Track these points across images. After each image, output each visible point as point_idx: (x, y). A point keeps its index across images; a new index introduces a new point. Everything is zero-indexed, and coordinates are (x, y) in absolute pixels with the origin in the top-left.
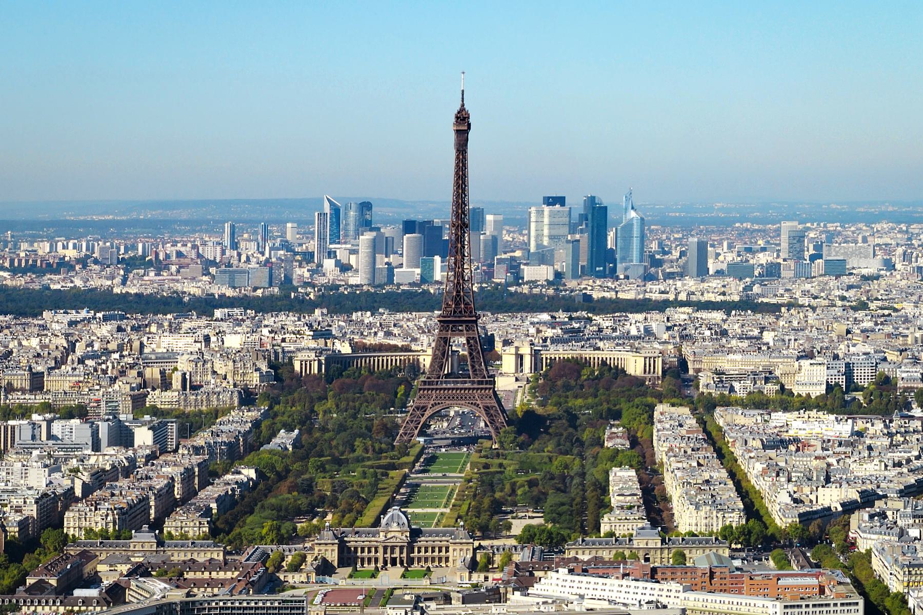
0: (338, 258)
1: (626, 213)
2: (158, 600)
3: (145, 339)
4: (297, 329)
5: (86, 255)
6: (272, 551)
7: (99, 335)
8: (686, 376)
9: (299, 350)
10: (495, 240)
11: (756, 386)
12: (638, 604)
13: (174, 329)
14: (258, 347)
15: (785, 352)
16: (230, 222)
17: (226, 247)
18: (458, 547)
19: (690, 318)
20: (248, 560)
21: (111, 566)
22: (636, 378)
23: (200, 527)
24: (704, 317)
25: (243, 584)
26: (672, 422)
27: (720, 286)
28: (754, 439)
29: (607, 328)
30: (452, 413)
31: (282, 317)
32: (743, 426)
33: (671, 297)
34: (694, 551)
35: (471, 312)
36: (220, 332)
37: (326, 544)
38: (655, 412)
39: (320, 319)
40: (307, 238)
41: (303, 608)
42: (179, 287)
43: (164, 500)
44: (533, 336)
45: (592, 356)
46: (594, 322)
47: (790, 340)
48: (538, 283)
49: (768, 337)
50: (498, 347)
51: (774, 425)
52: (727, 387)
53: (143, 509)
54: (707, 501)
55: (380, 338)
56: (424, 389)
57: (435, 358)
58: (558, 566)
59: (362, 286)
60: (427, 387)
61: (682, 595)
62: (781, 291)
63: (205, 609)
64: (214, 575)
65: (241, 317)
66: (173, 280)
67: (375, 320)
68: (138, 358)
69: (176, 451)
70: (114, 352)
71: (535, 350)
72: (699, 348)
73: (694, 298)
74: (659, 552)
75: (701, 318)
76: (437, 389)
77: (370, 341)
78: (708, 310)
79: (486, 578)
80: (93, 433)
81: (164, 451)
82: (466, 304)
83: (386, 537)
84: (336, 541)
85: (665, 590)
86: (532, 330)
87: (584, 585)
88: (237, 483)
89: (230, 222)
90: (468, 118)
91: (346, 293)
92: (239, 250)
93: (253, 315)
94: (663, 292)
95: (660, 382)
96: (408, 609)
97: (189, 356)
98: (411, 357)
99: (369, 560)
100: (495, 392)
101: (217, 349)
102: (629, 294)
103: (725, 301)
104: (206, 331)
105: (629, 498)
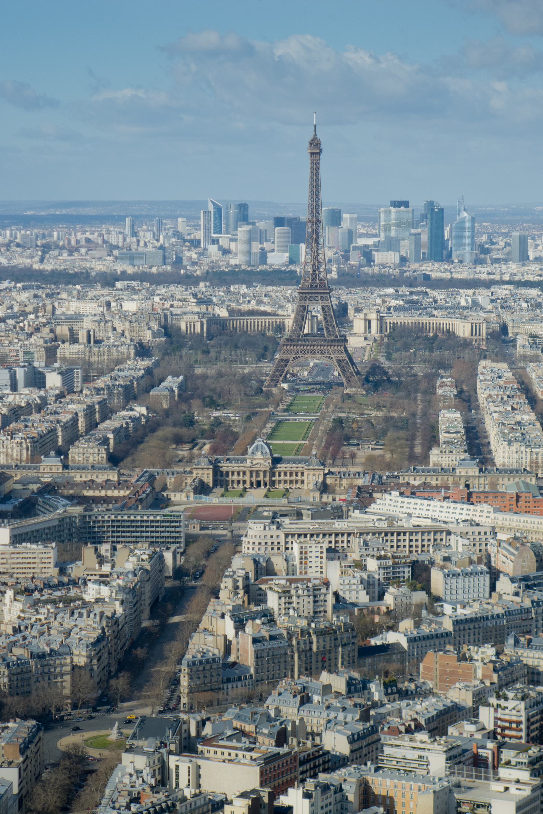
0: (220, 244)
2: (60, 514)
3: (56, 304)
5: (10, 240)
6: (158, 473)
7: (18, 300)
8: (506, 338)
9: (185, 313)
10: (350, 232)
12: (456, 522)
13: (81, 297)
14: (150, 311)
18: (311, 473)
19: (511, 293)
20: (137, 481)
21: (24, 485)
22: (465, 340)
23: (98, 454)
24: (523, 292)
25: (133, 501)
26: (493, 375)
30: (312, 364)
31: (172, 288)
33: (497, 277)
34: (506, 479)
36: (119, 299)
37: (203, 469)
39: (204, 290)
40: (196, 229)
41: (180, 521)
42: (88, 265)
44: (379, 305)
50: (351, 312)
53: (51, 438)
55: (253, 305)
57: (296, 320)
58: (392, 489)
59: (241, 265)
60: (289, 343)
61: (492, 515)
63: (99, 521)
64: (110, 493)
66: (82, 259)
67: (250, 292)
68: (50, 319)
70: (30, 313)
73: (516, 278)
74: (477, 479)
77: (246, 307)
79: (334, 500)
80: (11, 376)
81: (71, 391)
82: (321, 280)
83: (252, 463)
84: (211, 467)
85: (479, 511)
86: (379, 301)
87: (412, 506)
88: (130, 418)
90: (320, 144)
91: (227, 270)
92: (138, 238)
94: (489, 273)
95: (484, 343)
96: (267, 524)
98: (278, 321)
100: (346, 350)
101: (116, 312)
102: (462, 274)
104: (108, 298)
105: (454, 435)
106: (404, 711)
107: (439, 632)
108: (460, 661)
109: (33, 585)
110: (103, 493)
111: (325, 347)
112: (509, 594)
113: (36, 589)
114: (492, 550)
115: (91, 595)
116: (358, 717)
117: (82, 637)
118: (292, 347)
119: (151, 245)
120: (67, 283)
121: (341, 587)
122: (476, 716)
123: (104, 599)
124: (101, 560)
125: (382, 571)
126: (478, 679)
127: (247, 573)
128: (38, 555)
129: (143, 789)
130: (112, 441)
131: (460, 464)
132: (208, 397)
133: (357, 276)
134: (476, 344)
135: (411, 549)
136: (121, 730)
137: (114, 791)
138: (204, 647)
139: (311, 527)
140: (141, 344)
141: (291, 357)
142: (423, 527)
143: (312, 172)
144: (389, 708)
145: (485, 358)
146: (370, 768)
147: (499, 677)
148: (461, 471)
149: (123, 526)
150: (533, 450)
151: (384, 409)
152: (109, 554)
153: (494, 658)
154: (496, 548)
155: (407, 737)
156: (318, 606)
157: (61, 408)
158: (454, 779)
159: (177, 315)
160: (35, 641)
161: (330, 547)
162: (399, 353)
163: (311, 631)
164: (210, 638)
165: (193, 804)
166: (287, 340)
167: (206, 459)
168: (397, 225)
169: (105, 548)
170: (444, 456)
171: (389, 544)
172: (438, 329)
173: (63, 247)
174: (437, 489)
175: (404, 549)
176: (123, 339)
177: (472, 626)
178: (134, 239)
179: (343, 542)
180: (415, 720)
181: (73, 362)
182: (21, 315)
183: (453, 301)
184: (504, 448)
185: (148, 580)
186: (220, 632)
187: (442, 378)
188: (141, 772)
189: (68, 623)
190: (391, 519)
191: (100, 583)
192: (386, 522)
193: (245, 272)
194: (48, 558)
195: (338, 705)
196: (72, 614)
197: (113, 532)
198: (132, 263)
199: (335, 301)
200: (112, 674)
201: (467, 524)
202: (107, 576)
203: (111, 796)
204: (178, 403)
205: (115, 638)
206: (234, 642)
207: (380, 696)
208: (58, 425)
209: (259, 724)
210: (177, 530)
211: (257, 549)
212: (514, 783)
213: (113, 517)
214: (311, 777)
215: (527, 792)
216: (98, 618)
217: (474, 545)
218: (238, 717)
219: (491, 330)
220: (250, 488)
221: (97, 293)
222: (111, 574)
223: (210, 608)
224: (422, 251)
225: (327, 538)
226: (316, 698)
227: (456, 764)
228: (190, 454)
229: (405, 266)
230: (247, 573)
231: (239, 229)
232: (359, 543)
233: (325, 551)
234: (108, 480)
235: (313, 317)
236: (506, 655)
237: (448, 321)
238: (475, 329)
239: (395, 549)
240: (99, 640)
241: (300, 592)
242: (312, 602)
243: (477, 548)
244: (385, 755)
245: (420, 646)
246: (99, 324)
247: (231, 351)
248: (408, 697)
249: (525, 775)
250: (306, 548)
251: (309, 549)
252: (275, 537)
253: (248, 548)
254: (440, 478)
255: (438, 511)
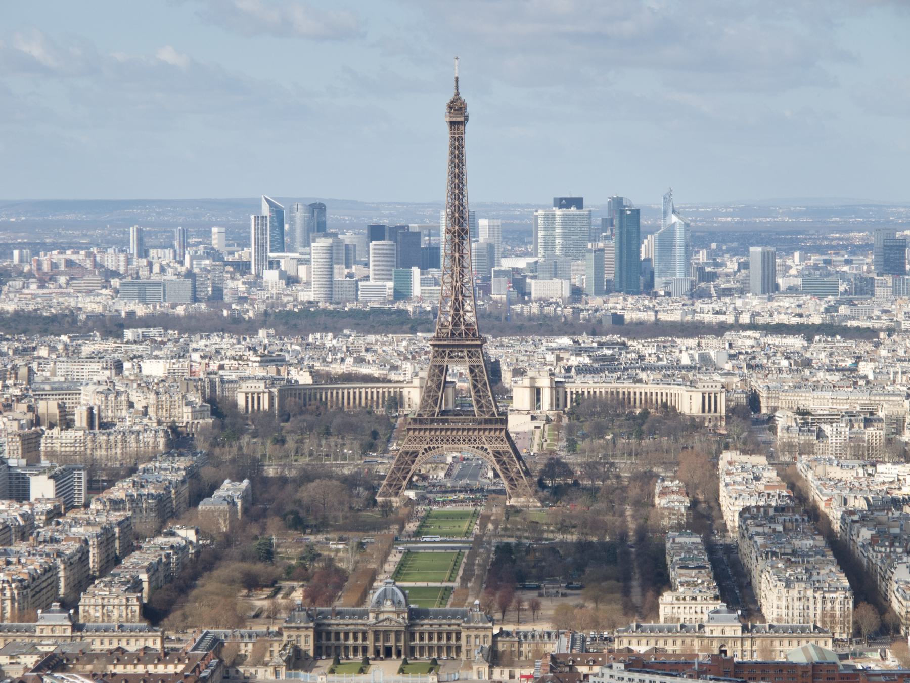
1: (665, 217)
3: (35, 366)
4: (239, 354)
6: (226, 637)
11: (854, 430)
13: (72, 353)
14: (187, 376)
15: (890, 388)
16: (136, 227)
17: (132, 255)
18: (473, 634)
19: (759, 344)
20: (195, 649)
21: (12, 657)
22: (692, 419)
23: (127, 606)
26: (745, 475)
27: (793, 306)
28: (856, 497)
29: (650, 355)
30: (449, 460)
31: (215, 338)
32: (840, 480)
33: (730, 319)
34: (786, 642)
35: (474, 335)
37: (298, 628)
38: (721, 462)
39: (266, 341)
42: (72, 302)
43: (76, 570)
44: (552, 365)
45: (632, 391)
46: (632, 348)
47: (896, 373)
48: (551, 300)
49: (866, 369)
50: (506, 377)
51: (881, 480)
52: (814, 431)
53: (49, 581)
54: (800, 577)
55: (348, 366)
56: (415, 430)
59: (318, 302)
60: (418, 426)
62: (877, 313)
65: (159, 339)
66: (61, 293)
68: (27, 389)
69: (87, 506)
71: (556, 382)
72: (774, 381)
73: (760, 320)
74: (739, 643)
75: (774, 345)
76: (431, 430)
77: (337, 369)
78: (794, 335)
81: (70, 507)
82: (467, 325)
84: (312, 625)
86: (550, 358)
88: (172, 547)
89: (136, 227)
90: (465, 108)
91: (296, 310)
92: (150, 259)
93: (177, 336)
94: (717, 313)
95: (724, 423)
97: (96, 386)
98: (392, 390)
99: (356, 649)
101: (132, 378)
102: (673, 314)
103: (802, 324)
104: (116, 355)
111: (476, 433)
118: (422, 433)
120: (45, 332)
130: (145, 585)
131: (711, 619)
132: (292, 512)
133: (506, 318)
134: (711, 425)
140: (174, 428)
141: (420, 448)
145: (727, 447)
148: (713, 630)
150: (827, 595)
151: (573, 530)
157: (61, 532)
159: (231, 382)
162: (588, 440)
166: (414, 420)
167: (303, 614)
168: (565, 236)
170: (682, 606)
172: (648, 402)
173: (30, 275)
176: (145, 421)
178: (144, 261)
181: (65, 458)
183: (668, 357)
184: (779, 592)
187: (663, 480)
193: (325, 311)
198: (143, 299)
204: (243, 526)
208: (59, 560)
219: (733, 403)
220: (374, 659)
228: (274, 603)
229: (580, 301)
231: (313, 245)
238: (708, 402)
246: (106, 396)
247: (320, 440)
254: (679, 642)
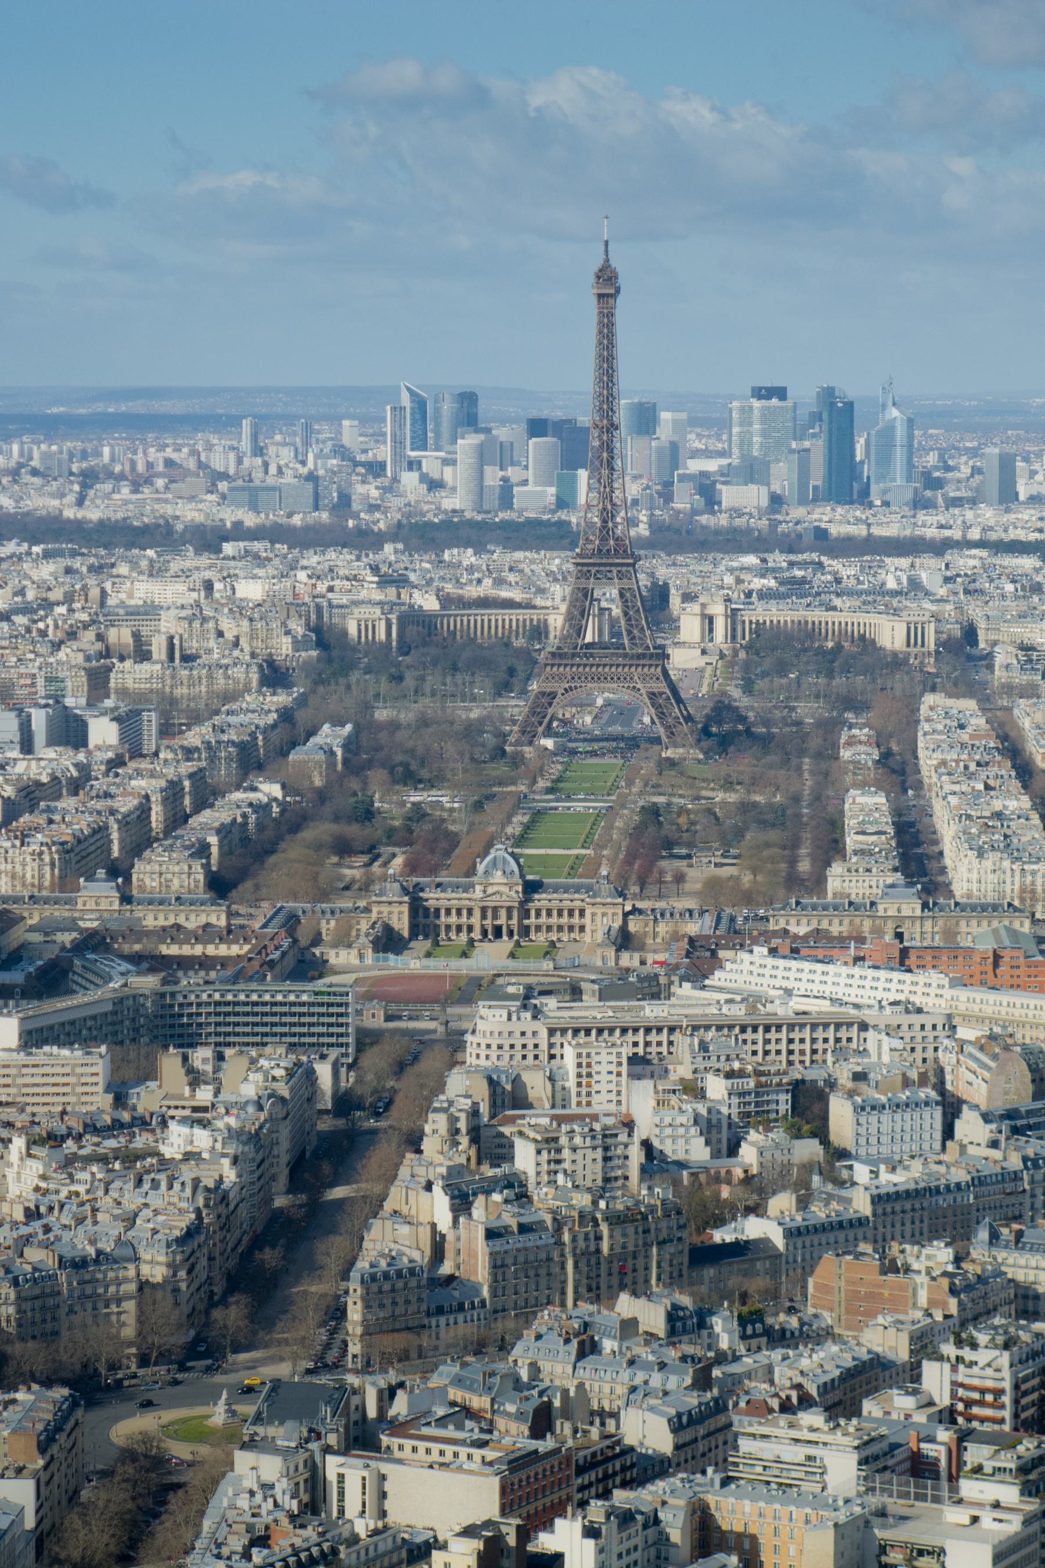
0: (424, 470)
3: (108, 586)
5: (18, 463)
6: (304, 912)
7: (35, 578)
8: (974, 652)
9: (356, 603)
10: (674, 447)
12: (877, 1006)
13: (155, 572)
14: (289, 599)
18: (599, 910)
19: (983, 564)
20: (264, 926)
21: (46, 934)
22: (895, 654)
23: (189, 874)
24: (1006, 563)
25: (256, 964)
26: (948, 722)
30: (600, 702)
31: (331, 554)
33: (956, 534)
34: (974, 923)
36: (229, 576)
37: (390, 903)
39: (393, 558)
40: (377, 441)
41: (347, 1004)
42: (169, 510)
44: (730, 588)
50: (675, 600)
53: (99, 844)
55: (486, 588)
57: (569, 617)
58: (755, 941)
59: (463, 511)
60: (557, 662)
61: (948, 993)
63: (191, 1004)
64: (211, 950)
66: (158, 499)
67: (480, 562)
68: (96, 614)
70: (58, 604)
73: (993, 536)
74: (918, 923)
77: (473, 592)
79: (643, 963)
80: (21, 725)
81: (137, 753)
82: (617, 539)
83: (485, 892)
84: (406, 899)
85: (921, 983)
86: (729, 580)
87: (792, 975)
88: (251, 805)
90: (616, 277)
91: (436, 520)
92: (266, 458)
94: (941, 527)
95: (932, 660)
96: (513, 1009)
98: (535, 617)
100: (666, 673)
101: (224, 601)
102: (890, 528)
104: (208, 574)
105: (874, 838)
106: (777, 1370)
107: (846, 1217)
108: (886, 1274)
109: (64, 1127)
110: (198, 950)
111: (626, 669)
112: (979, 1145)
113: (69, 1135)
114: (947, 1059)
115: (176, 1146)
116: (689, 1381)
117: (158, 1227)
118: (561, 669)
119: (290, 472)
120: (129, 546)
121: (657, 1131)
122: (917, 1378)
123: (200, 1153)
124: (195, 1079)
125: (735, 1100)
126: (921, 1309)
127: (475, 1104)
128: (73, 1070)
129: (276, 1521)
130: (215, 850)
131: (885, 894)
132: (401, 764)
133: (688, 532)
134: (917, 662)
135: (791, 1058)
136: (234, 1407)
137: (219, 1524)
138: (392, 1246)
139: (599, 1016)
140: (271, 663)
141: (559, 688)
142: (815, 1015)
143: (600, 332)
144: (749, 1364)
145: (933, 689)
146: (712, 1480)
147: (960, 1303)
148: (887, 908)
149: (237, 1014)
150: (1026, 867)
151: (738, 787)
152: (209, 1068)
153: (950, 1268)
154: (954, 1056)
155: (783, 1420)
156: (612, 1168)
157: (118, 786)
158: (874, 1501)
159: (341, 607)
160: (67, 1235)
161: (635, 1054)
162: (767, 680)
163: (599, 1216)
164: (404, 1230)
165: (372, 1549)
166: (553, 654)
167: (397, 885)
168: (765, 434)
169: (202, 1056)
170: (854, 879)
171: (749, 1047)
172: (843, 633)
173: (122, 477)
174: (842, 942)
175: (778, 1058)
176: (236, 653)
177: (908, 1206)
178: (259, 461)
179: (659, 1044)
180: (799, 1387)
182: (40, 607)
183: (871, 579)
184: (970, 863)
185: (285, 1118)
186: (424, 1218)
187: (850, 728)
188: (272, 1487)
189: (132, 1200)
190: (753, 1000)
191: (193, 1122)
192: (743, 1006)
193: (471, 524)
194: (93, 1074)
195: (651, 1358)
196: (139, 1182)
197: (217, 1024)
198: (254, 507)
199: (644, 580)
200: (216, 1298)
201: (898, 1009)
202: (205, 1109)
203: (214, 1533)
204: (342, 777)
205: (221, 1229)
206: (450, 1238)
207: (731, 1340)
208: (112, 818)
209: (498, 1394)
210: (341, 1020)
211: (494, 1057)
212: (988, 1508)
213: (217, 996)
214: (598, 1497)
215: (1013, 1525)
216: (188, 1191)
217: (913, 1050)
218: (458, 1382)
219: (945, 636)
220: (481, 941)
221: (187, 564)
222: (213, 1105)
223: (404, 1172)
224: (812, 483)
225: (630, 1037)
226: (608, 1345)
227: (878, 1471)
228: (366, 874)
229: (779, 512)
230: (475, 1104)
231: (459, 441)
232: (691, 1045)
233: (625, 1061)
234: (208, 925)
235: (602, 610)
236: (973, 1261)
237: (861, 618)
238: (915, 634)
239: (759, 1057)
240: (190, 1233)
241: (578, 1140)
242: (600, 1160)
243: (919, 1055)
244: (741, 1454)
245: (808, 1244)
246: (190, 623)
247: (445, 676)
248: (785, 1343)
249: (1010, 1493)
250: (588, 1055)
251: (595, 1058)
252: (529, 1034)
253: (478, 1056)
254: (846, 921)
255: (842, 984)
